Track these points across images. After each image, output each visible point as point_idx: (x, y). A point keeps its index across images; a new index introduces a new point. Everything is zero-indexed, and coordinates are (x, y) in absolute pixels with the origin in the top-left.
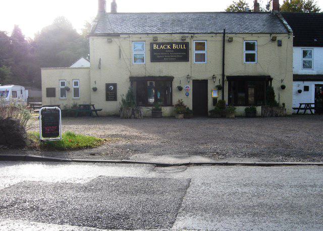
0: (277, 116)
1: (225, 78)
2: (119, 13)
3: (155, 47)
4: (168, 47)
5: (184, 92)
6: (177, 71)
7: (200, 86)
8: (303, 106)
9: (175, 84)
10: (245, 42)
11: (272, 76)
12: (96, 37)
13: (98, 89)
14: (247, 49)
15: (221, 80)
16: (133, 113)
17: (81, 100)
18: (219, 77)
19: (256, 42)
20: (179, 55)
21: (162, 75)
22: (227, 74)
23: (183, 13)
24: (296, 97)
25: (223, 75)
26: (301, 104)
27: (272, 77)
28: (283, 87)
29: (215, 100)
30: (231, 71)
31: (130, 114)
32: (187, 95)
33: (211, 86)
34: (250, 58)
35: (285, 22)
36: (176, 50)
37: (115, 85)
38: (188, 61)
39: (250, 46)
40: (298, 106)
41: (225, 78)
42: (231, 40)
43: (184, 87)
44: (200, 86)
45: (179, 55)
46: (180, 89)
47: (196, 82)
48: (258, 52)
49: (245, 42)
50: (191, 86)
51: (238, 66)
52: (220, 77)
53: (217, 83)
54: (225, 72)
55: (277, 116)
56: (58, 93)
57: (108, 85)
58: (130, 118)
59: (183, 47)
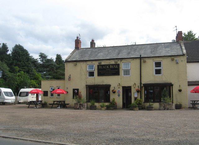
0: (168, 109)
1: (142, 85)
2: (96, 48)
3: (100, 67)
4: (107, 67)
5: (117, 94)
6: (111, 81)
7: (127, 90)
8: (55, 103)
9: (111, 89)
10: (154, 62)
11: (111, 85)
12: (68, 63)
13: (182, 90)
14: (156, 67)
15: (140, 86)
16: (80, 107)
17: (61, 98)
18: (138, 84)
19: (161, 61)
20: (114, 72)
21: (104, 84)
22: (143, 82)
23: (121, 46)
24: (188, 95)
25: (141, 83)
26: (54, 102)
27: (172, 84)
28: (180, 91)
29: (136, 99)
30: (145, 81)
31: (78, 107)
32: (119, 96)
33: (133, 90)
34: (158, 72)
35: (183, 48)
36: (112, 69)
37: (78, 90)
38: (119, 75)
39: (158, 64)
40: (52, 103)
41: (142, 85)
42: (173, 60)
43: (117, 90)
44: (127, 90)
45: (114, 72)
46: (114, 92)
47: (124, 88)
48: (163, 68)
49: (154, 62)
50: (121, 90)
51: (150, 77)
52: (139, 85)
53: (137, 88)
54: (142, 81)
55: (168, 109)
56: (49, 94)
57: (74, 90)
58: (78, 109)
59: (116, 67)
